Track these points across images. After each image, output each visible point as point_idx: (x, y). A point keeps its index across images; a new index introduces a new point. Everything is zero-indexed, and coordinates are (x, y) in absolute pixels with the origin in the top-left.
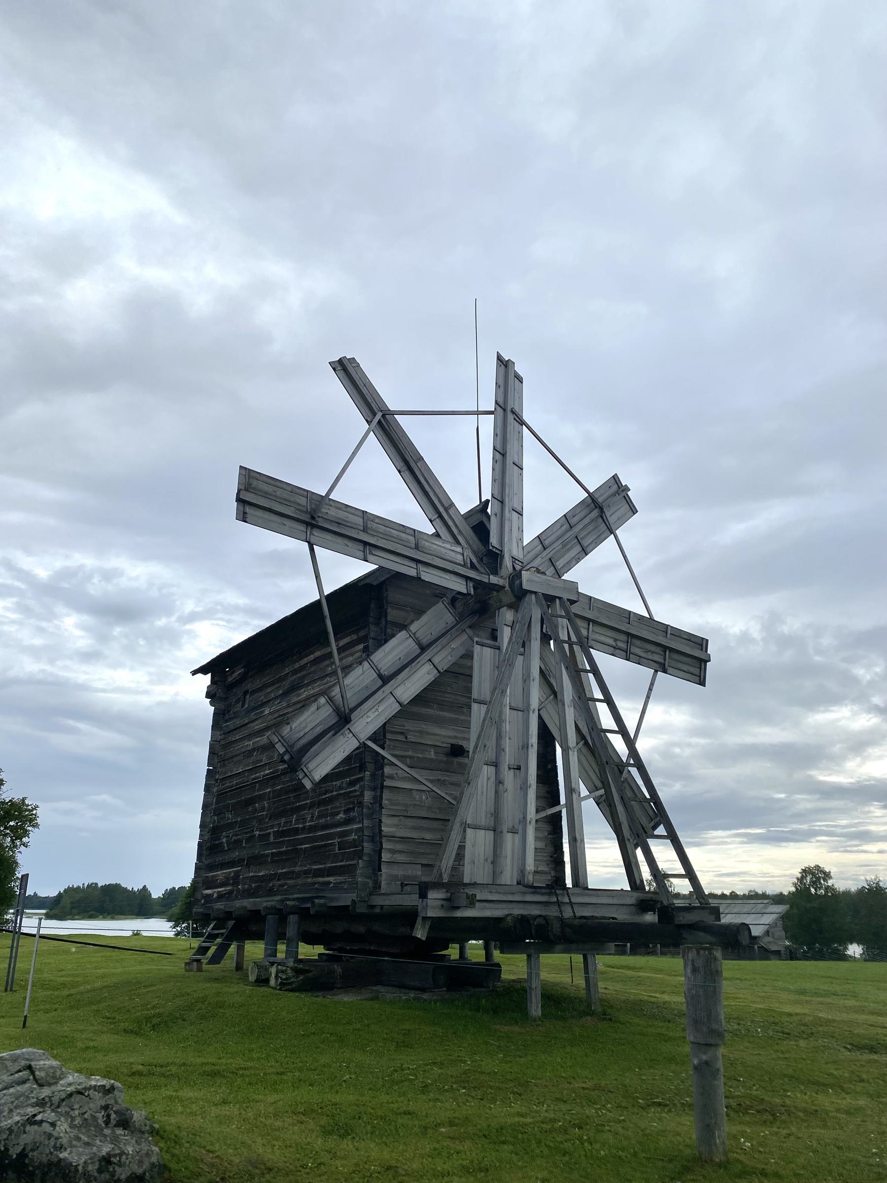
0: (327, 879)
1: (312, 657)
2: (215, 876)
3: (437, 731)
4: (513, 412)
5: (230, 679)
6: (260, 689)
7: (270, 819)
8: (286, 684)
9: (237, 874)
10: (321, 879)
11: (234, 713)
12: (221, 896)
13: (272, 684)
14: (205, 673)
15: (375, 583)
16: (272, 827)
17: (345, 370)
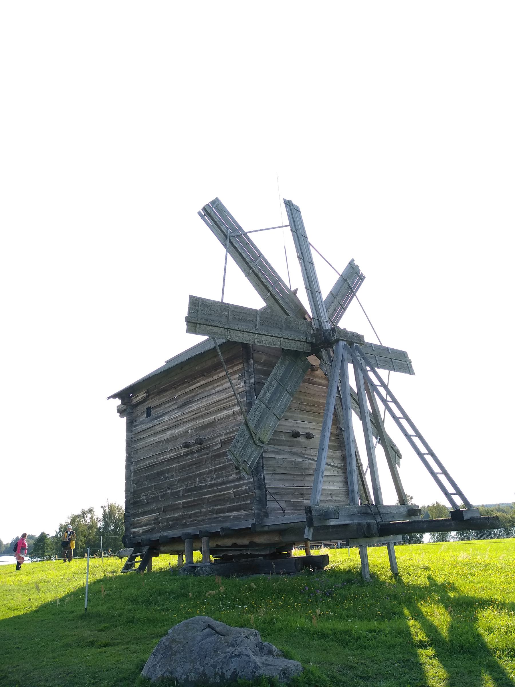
0: (227, 514)
1: (198, 385)
2: (139, 520)
6: (160, 406)
7: (178, 483)
9: (156, 519)
10: (222, 515)
11: (141, 421)
12: (145, 532)
13: (169, 402)
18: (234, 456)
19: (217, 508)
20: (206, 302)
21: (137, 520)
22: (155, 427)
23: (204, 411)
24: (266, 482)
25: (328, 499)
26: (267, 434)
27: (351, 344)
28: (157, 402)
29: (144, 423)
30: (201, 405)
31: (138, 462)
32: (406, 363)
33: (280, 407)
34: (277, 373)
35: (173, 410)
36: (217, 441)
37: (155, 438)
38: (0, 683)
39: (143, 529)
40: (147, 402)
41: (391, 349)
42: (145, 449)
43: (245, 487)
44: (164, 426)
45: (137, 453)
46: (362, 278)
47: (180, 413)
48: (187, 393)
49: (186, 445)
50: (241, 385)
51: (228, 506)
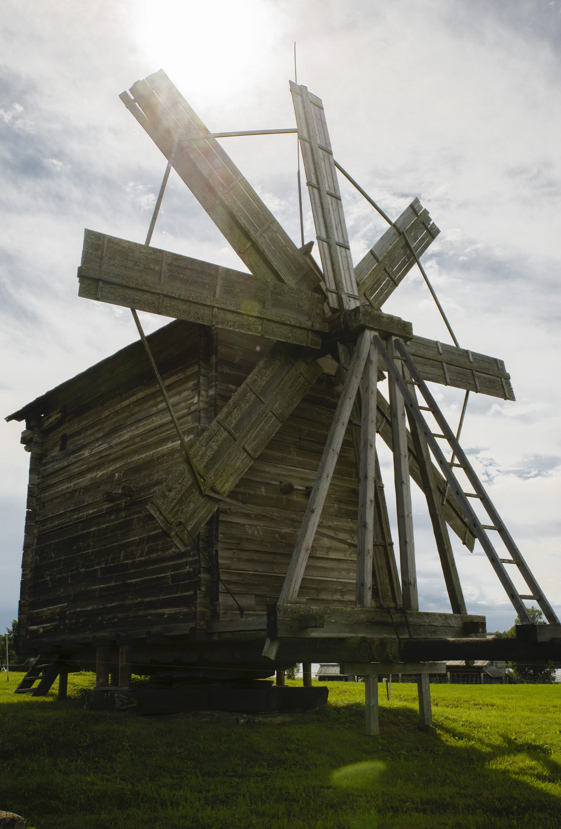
0: (161, 611)
1: (134, 398)
5: (46, 424)
6: (78, 433)
10: (153, 611)
11: (52, 457)
12: (47, 632)
13: (91, 426)
16: (99, 564)
18: (161, 513)
19: (146, 600)
21: (38, 613)
22: (70, 468)
23: (138, 443)
24: (220, 561)
25: (335, 597)
26: (227, 481)
27: (386, 336)
28: (76, 427)
29: (56, 460)
30: (136, 432)
31: (43, 522)
32: (499, 379)
33: (256, 437)
34: (255, 380)
35: (97, 440)
36: (154, 492)
37: (69, 485)
39: (44, 627)
40: (62, 427)
41: (474, 354)
42: (56, 501)
43: (188, 569)
44: (82, 465)
45: (44, 507)
46: (433, 233)
47: (105, 446)
48: (117, 413)
49: (109, 498)
50: (196, 400)
51: (161, 597)
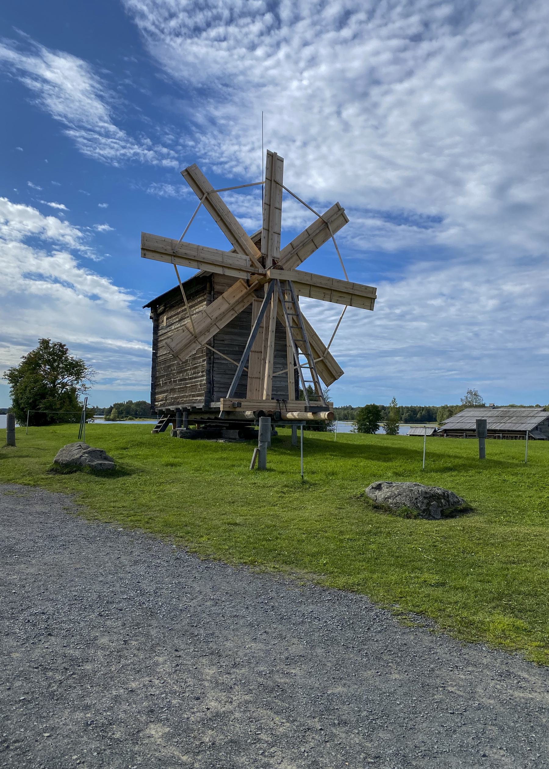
0: (196, 398)
3: (240, 339)
4: (275, 181)
8: (180, 316)
10: (194, 398)
13: (175, 315)
14: (149, 307)
15: (208, 275)
17: (189, 174)
20: (199, 277)
38: (0, 717)
47: (179, 325)
